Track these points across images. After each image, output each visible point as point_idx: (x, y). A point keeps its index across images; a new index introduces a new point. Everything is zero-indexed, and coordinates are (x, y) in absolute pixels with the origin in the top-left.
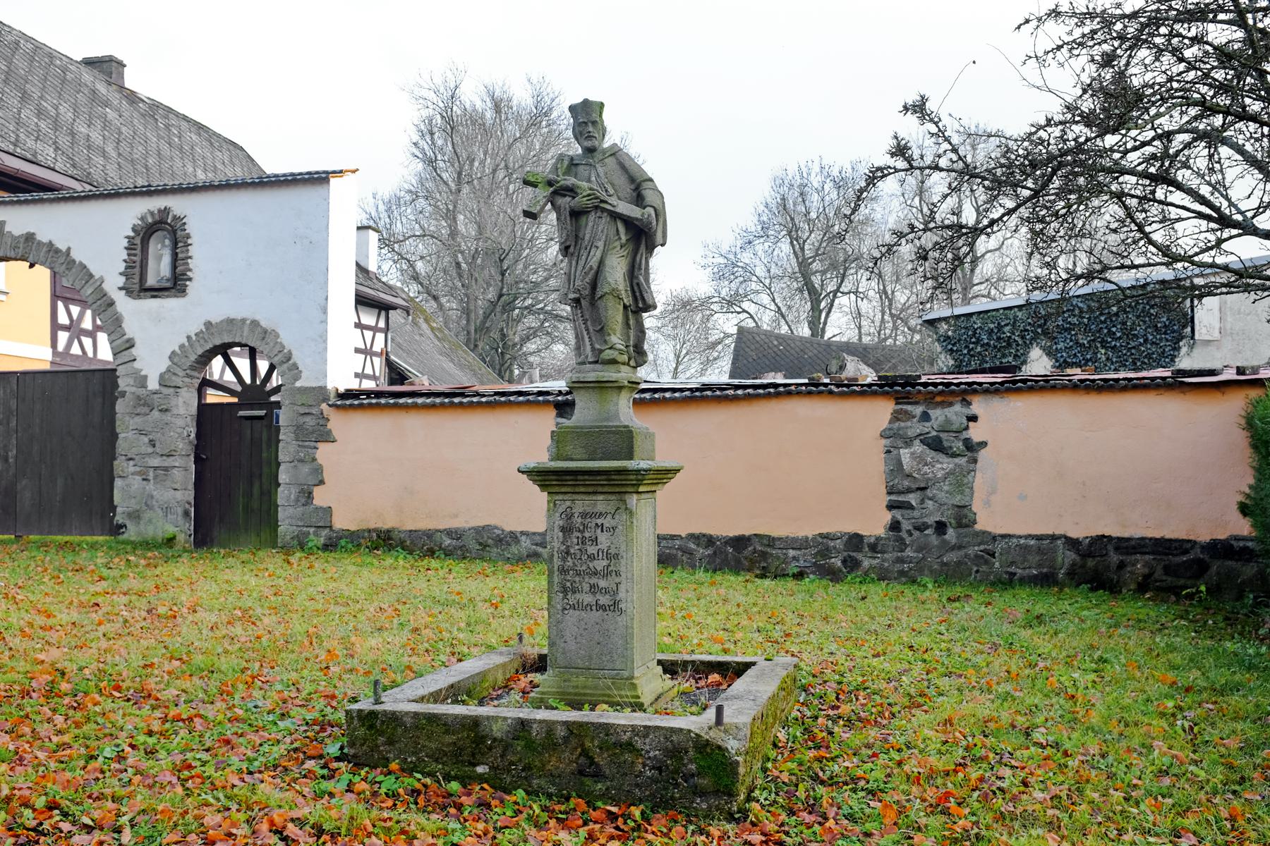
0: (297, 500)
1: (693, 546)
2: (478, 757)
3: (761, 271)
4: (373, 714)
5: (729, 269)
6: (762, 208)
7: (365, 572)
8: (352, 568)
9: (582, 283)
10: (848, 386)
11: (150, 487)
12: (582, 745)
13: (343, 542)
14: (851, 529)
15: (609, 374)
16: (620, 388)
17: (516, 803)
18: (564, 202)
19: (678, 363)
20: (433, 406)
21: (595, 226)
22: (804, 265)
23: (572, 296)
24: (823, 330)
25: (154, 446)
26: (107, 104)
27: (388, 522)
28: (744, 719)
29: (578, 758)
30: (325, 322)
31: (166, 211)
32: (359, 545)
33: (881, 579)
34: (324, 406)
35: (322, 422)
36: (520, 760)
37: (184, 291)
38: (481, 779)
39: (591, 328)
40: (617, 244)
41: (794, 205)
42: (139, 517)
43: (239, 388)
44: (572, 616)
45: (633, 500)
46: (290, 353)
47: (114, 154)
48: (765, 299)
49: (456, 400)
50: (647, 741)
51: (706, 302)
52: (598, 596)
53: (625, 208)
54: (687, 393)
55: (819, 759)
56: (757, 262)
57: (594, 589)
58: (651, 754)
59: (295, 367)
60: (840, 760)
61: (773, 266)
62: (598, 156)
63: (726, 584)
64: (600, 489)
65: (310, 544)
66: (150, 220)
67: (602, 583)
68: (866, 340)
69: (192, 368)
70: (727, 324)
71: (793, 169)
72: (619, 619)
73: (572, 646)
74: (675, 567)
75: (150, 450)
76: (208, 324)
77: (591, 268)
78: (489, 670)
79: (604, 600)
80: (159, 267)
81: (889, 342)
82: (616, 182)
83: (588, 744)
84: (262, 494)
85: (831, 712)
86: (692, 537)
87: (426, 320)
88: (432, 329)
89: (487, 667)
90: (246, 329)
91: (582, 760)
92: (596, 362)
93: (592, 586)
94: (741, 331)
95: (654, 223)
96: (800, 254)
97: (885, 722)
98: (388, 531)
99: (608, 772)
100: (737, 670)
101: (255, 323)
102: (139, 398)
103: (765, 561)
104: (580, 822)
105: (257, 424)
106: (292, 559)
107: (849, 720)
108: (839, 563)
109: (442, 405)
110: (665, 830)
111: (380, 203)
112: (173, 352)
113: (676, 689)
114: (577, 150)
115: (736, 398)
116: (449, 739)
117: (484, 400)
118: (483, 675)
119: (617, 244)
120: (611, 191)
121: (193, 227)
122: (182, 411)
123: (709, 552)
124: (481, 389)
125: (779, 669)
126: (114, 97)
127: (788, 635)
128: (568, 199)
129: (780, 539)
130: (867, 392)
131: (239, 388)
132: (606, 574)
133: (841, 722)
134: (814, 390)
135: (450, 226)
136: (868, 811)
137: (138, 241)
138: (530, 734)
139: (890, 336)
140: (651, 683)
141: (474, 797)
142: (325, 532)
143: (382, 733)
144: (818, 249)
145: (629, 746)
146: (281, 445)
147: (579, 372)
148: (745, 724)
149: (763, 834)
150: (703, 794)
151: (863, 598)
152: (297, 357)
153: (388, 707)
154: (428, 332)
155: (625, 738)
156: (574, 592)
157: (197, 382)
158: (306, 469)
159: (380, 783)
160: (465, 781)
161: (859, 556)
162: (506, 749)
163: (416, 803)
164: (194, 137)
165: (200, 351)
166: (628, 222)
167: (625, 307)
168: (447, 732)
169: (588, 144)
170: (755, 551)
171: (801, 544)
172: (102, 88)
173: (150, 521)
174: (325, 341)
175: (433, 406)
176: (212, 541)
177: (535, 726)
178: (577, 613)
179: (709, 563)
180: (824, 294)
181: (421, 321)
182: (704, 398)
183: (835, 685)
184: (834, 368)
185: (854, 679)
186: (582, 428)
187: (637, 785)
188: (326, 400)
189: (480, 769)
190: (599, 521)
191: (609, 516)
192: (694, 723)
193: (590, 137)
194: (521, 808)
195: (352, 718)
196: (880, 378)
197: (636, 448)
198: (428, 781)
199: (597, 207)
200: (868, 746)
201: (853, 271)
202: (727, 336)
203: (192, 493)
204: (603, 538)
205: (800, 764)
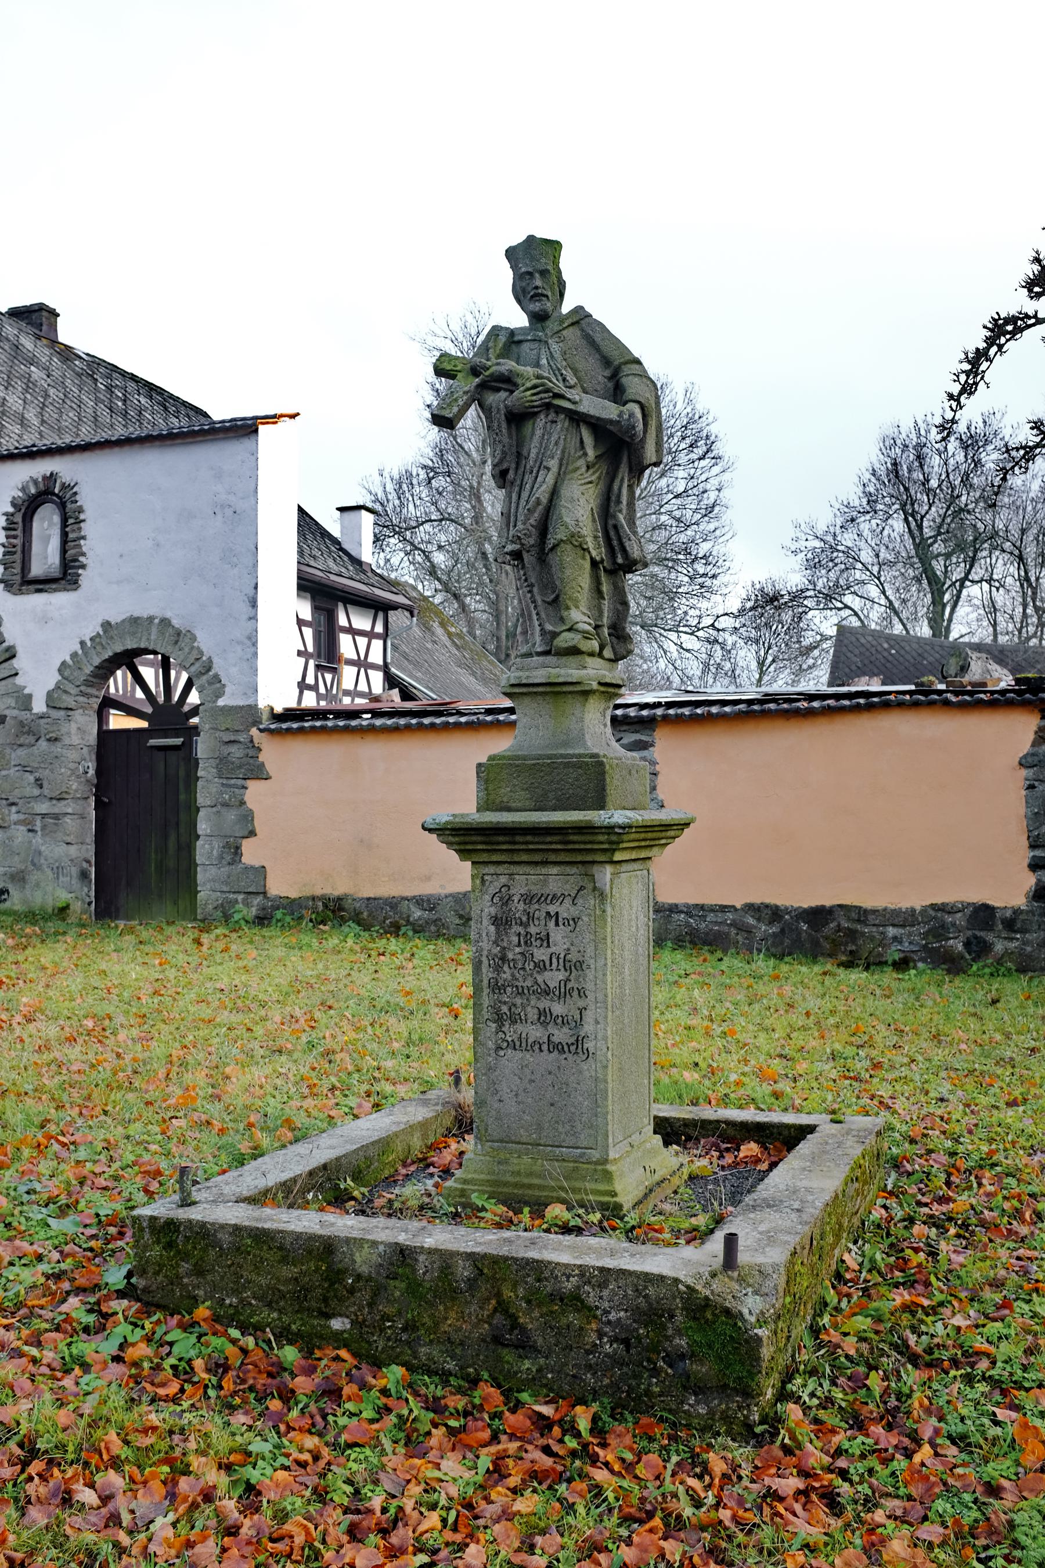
0: (221, 857)
1: (751, 921)
2: (333, 1303)
3: (866, 556)
4: (171, 1225)
5: (825, 554)
6: (868, 476)
7: (294, 957)
8: (280, 952)
9: (526, 525)
10: (971, 693)
11: (38, 840)
12: (499, 1295)
13: (279, 914)
14: (976, 896)
15: (568, 671)
16: (586, 694)
17: (385, 1392)
18: (496, 399)
19: (762, 673)
20: (396, 729)
21: (546, 437)
22: (922, 547)
23: (510, 548)
24: (948, 629)
25: (41, 787)
26: (32, 361)
27: (338, 887)
28: (776, 1256)
29: (491, 1316)
30: (254, 618)
31: (52, 478)
32: (301, 918)
33: (1022, 970)
34: (254, 731)
35: (251, 753)
36: (399, 1313)
37: (76, 582)
38: (338, 1340)
39: (539, 599)
40: (581, 463)
41: (909, 471)
42: (23, 880)
43: (149, 710)
44: (512, 1059)
45: (605, 874)
46: (210, 660)
47: (36, 422)
48: (873, 591)
49: (426, 721)
50: (605, 1293)
51: (797, 596)
52: (552, 1029)
54: (742, 707)
55: (909, 1308)
56: (862, 544)
57: (544, 1017)
58: (613, 1316)
59: (217, 679)
60: (946, 1311)
61: (883, 549)
62: (552, 325)
63: (794, 978)
64: (552, 857)
65: (237, 917)
66: (33, 491)
67: (558, 1009)
68: (1003, 639)
69: (88, 683)
70: (824, 623)
71: (907, 426)
72: (585, 1066)
73: (511, 1106)
74: (725, 951)
75: (36, 792)
76: (107, 625)
77: (538, 502)
78: (396, 1134)
79: (561, 1035)
80: (46, 556)
81: (1034, 642)
82: (580, 366)
83: (507, 1293)
84: (179, 848)
85: (937, 1209)
86: (750, 908)
87: (442, 624)
88: (450, 635)
89: (395, 1129)
90: (154, 630)
91: (499, 1319)
92: (547, 653)
93: (542, 1013)
94: (841, 629)
95: (640, 427)
96: (916, 533)
97: (1024, 1230)
98: (340, 899)
99: (540, 1341)
100: (784, 1139)
101: (165, 622)
102: (22, 724)
103: (854, 942)
104: (486, 1435)
105: (173, 756)
106: (205, 938)
107: (965, 1226)
108: (960, 947)
109: (408, 727)
110: (629, 1456)
111: (388, 480)
112: (64, 663)
113: (686, 1171)
114: (517, 318)
115: (810, 713)
116: (288, 1271)
117: (463, 719)
118: (384, 1144)
119: (581, 463)
120: (572, 380)
121: (87, 498)
122: (75, 740)
123: (774, 929)
124: (461, 706)
125: (850, 1141)
126: (43, 353)
127: (877, 1066)
128: (503, 394)
129: (874, 912)
130: (1000, 702)
131: (149, 710)
132: (564, 993)
133: (953, 1231)
134: (923, 700)
135: (474, 507)
136: (995, 1431)
137: (18, 518)
138: (414, 1270)
139: (1035, 635)
140: (638, 1165)
141: (318, 1378)
142: (257, 900)
143: (185, 1256)
144: (939, 527)
145: (575, 1301)
146: (200, 783)
147: (522, 669)
148: (775, 1267)
149: (804, 1473)
150: (700, 1390)
151: (995, 1002)
152: (219, 667)
153: (194, 1214)
154: (445, 639)
155: (569, 1285)
156: (514, 1022)
157: (95, 703)
158: (231, 815)
159: (171, 1344)
160: (309, 1344)
161: (990, 937)
162: (376, 1294)
163: (220, 1387)
164: (143, 400)
165: (97, 661)
166: (598, 427)
167: (594, 564)
168: (284, 1260)
169: (536, 306)
170: (839, 929)
171: (906, 918)
172: (27, 343)
173: (37, 885)
174: (255, 644)
175: (396, 729)
176: (117, 910)
177: (422, 1258)
178: (519, 1055)
179: (774, 944)
180: (948, 583)
181: (436, 625)
182: (765, 714)
183: (945, 1159)
184: (952, 668)
185: (975, 1147)
186: (524, 758)
187: (589, 1367)
188: (256, 723)
189: (337, 1324)
190: (552, 909)
191: (568, 901)
192: (687, 1263)
193: (537, 296)
194: (390, 1402)
195: (142, 1230)
196: (1018, 681)
197: (610, 790)
198: (250, 1342)
199: (548, 406)
200: (997, 1284)
201: (985, 553)
202: (825, 638)
203: (92, 848)
204: (559, 937)
205: (879, 1320)
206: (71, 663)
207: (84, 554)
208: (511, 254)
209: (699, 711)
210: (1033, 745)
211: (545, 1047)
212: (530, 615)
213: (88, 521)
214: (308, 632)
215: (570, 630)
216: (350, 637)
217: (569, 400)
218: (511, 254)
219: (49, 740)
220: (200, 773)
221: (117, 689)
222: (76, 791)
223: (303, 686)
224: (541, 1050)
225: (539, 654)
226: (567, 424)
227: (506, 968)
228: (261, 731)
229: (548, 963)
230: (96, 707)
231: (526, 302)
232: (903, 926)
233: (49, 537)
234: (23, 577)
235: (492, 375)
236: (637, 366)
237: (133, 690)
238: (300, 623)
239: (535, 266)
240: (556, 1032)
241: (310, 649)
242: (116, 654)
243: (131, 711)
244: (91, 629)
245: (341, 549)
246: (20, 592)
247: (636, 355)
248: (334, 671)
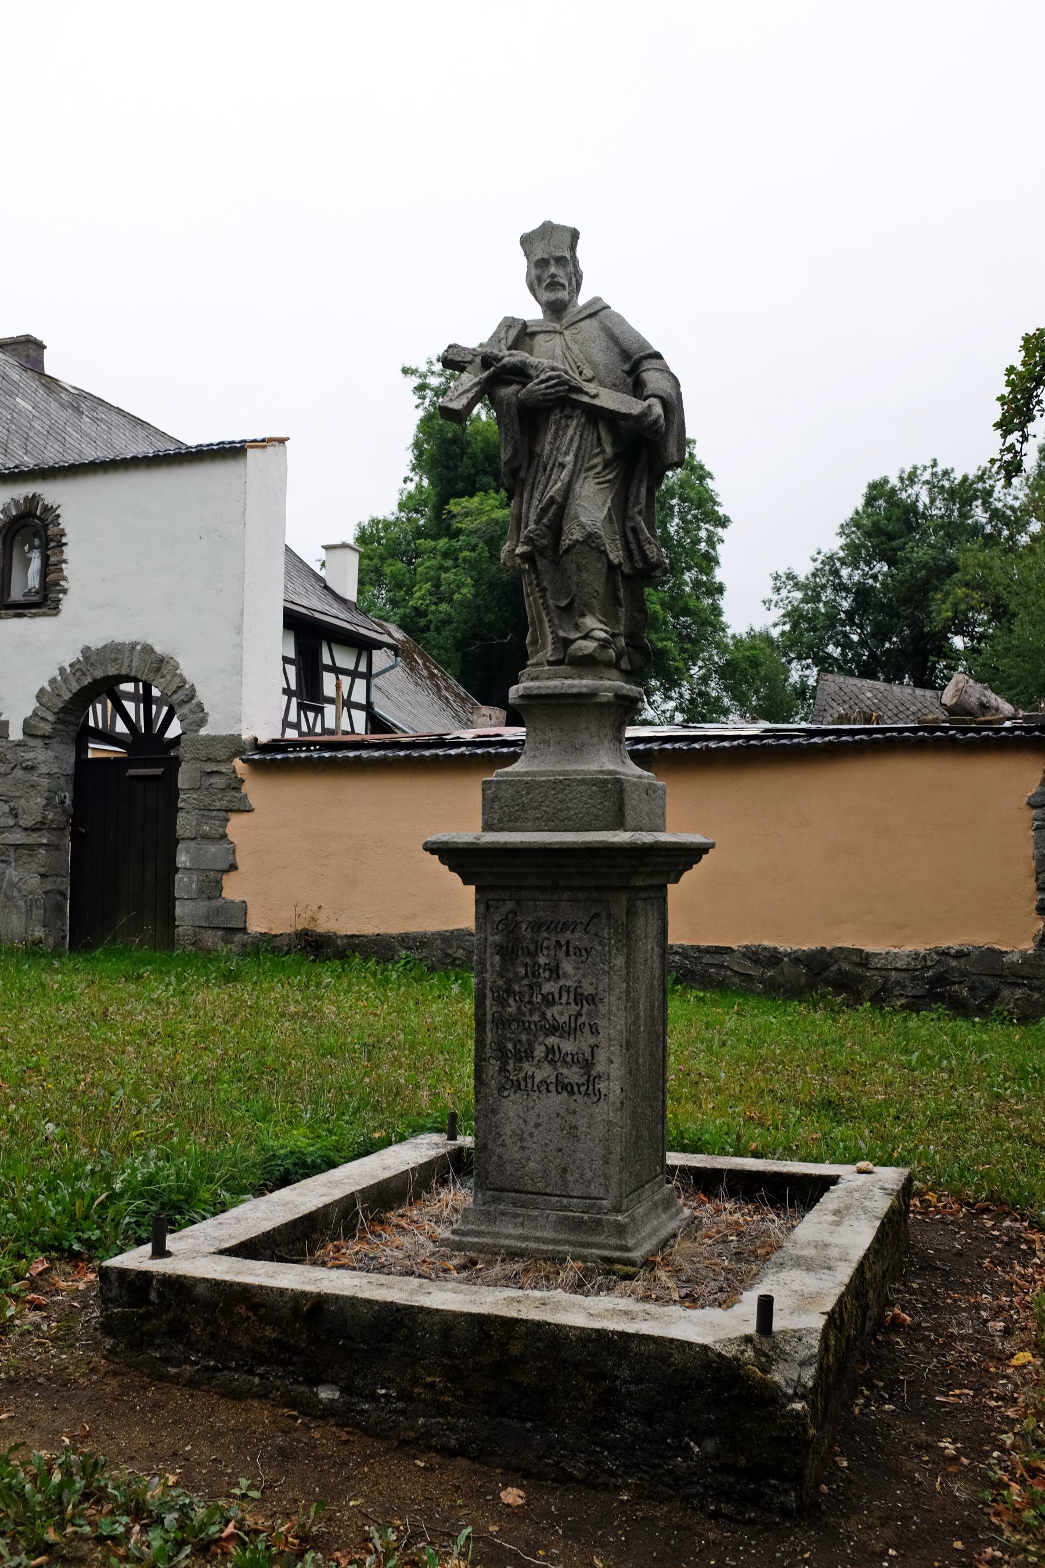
25: (16, 816)
30: (240, 645)
39: (551, 602)
46: (193, 689)
53: (610, 400)
59: (200, 707)
67: (568, 1046)
75: (11, 822)
79: (573, 1075)
93: (550, 1050)
101: (148, 649)
112: (42, 690)
114: (531, 311)
128: (514, 387)
152: (203, 695)
165: (75, 687)
169: (550, 296)
189: (326, 1394)
197: (629, 812)
206: (49, 689)
207: (65, 579)
208: (526, 241)
209: (697, 746)
211: (552, 1088)
212: (541, 622)
214: (291, 670)
216: (333, 675)
217: (587, 394)
218: (526, 241)
219: (25, 769)
220: (180, 805)
222: (52, 821)
223: (286, 724)
224: (549, 1091)
225: (550, 663)
226: (583, 420)
227: (511, 1001)
228: (243, 761)
229: (557, 996)
230: (74, 734)
231: (541, 292)
236: (658, 361)
238: (286, 660)
239: (552, 258)
240: (565, 1071)
241: (293, 687)
242: (96, 681)
244: (70, 655)
245: (326, 587)
247: (657, 347)
248: (319, 711)
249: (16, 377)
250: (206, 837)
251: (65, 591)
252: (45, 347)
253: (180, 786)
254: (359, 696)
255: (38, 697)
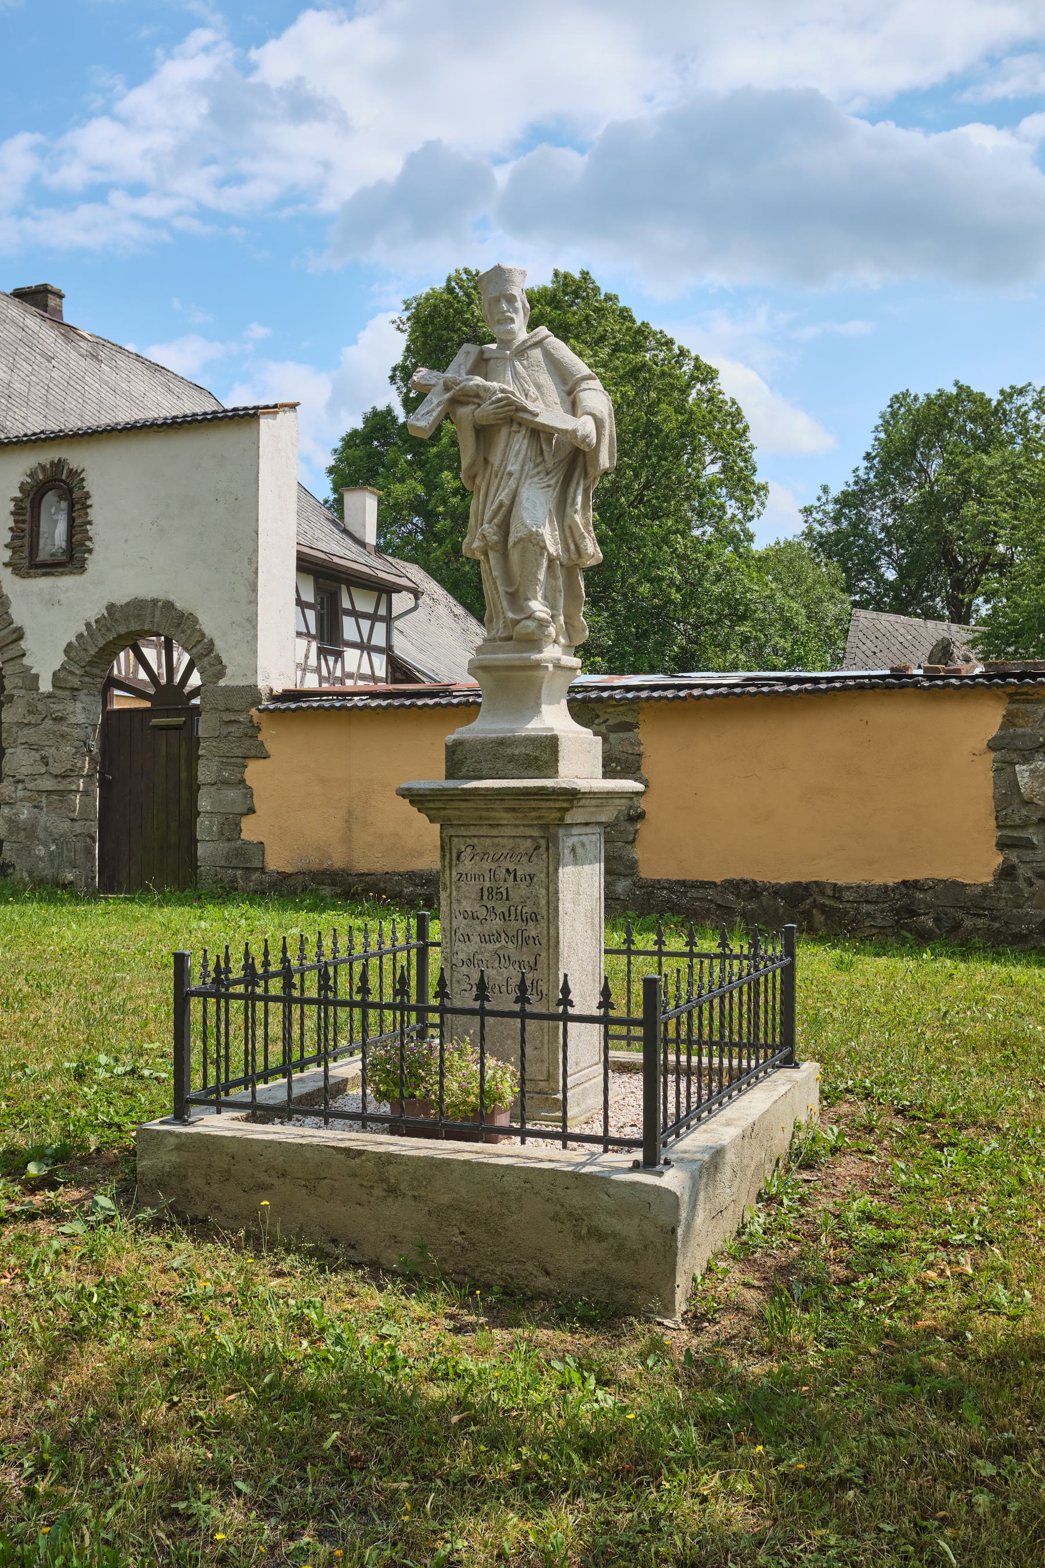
30: (254, 602)
31: (59, 465)
34: (253, 711)
46: (211, 643)
59: (218, 660)
77: (501, 505)
101: (169, 605)
108: (930, 923)
112: (70, 645)
122: (81, 719)
129: (849, 888)
131: (151, 691)
137: (27, 504)
152: (221, 646)
157: (100, 682)
165: (101, 643)
174: (255, 627)
207: (90, 539)
210: (1001, 729)
213: (94, 507)
214: (311, 614)
215: (527, 618)
219: (55, 719)
220: (200, 752)
221: (119, 670)
230: (100, 686)
232: (876, 903)
233: (56, 521)
234: (31, 561)
235: (462, 389)
237: (136, 671)
241: (313, 631)
243: (140, 694)
244: (94, 611)
246: (26, 576)
249: (36, 329)
250: (225, 782)
251: (90, 551)
252: (61, 297)
253: (200, 734)
254: (379, 639)
255: (65, 651)
